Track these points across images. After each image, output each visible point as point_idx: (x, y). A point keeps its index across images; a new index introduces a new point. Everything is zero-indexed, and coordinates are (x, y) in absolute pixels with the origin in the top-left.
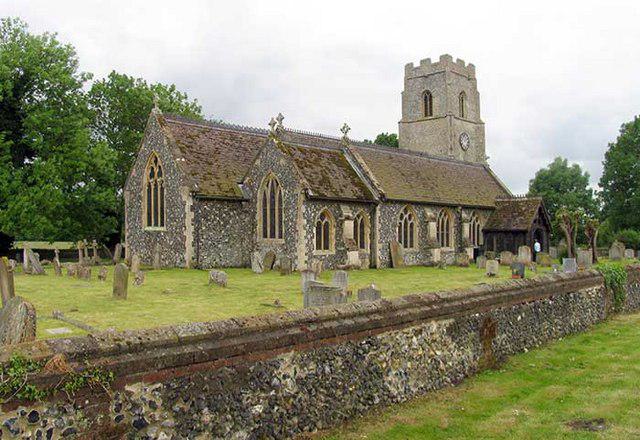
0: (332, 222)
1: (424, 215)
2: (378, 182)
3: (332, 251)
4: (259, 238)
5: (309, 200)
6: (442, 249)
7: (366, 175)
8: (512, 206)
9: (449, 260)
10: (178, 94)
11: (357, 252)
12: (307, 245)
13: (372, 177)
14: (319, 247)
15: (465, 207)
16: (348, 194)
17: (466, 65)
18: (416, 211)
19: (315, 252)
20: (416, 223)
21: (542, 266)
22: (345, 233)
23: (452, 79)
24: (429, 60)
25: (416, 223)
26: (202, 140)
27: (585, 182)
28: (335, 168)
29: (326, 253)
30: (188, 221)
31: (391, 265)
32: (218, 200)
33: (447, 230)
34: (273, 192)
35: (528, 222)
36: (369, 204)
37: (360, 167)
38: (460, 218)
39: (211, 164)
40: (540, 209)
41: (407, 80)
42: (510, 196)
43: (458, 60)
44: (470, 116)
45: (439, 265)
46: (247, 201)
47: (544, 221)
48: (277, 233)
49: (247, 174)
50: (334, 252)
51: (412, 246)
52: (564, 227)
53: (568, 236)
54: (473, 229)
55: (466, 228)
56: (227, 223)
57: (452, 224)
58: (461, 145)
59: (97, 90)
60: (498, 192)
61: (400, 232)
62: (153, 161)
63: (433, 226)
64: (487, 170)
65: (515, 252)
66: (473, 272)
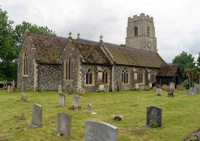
0: (93, 73)
1: (132, 71)
2: (113, 58)
3: (93, 85)
4: (65, 79)
5: (83, 64)
6: (140, 84)
7: (108, 54)
8: (167, 67)
9: (142, 88)
10: (49, 30)
11: (103, 85)
12: (82, 82)
13: (111, 55)
14: (87, 83)
15: (149, 68)
16: (100, 62)
17: (150, 17)
18: (129, 69)
19: (85, 85)
20: (129, 74)
21: (179, 90)
22: (98, 77)
23: (145, 22)
24: (136, 15)
25: (129, 74)
26: (45, 42)
27: (193, 60)
28: (96, 51)
29: (91, 85)
30: (35, 73)
31: (118, 90)
32: (48, 64)
33: (142, 76)
34: (70, 61)
35: (173, 73)
36: (109, 66)
37: (106, 52)
38: (147, 72)
39: (47, 51)
40: (178, 68)
41: (128, 23)
42: (166, 64)
43: (147, 15)
44: (151, 36)
45: (137, 90)
46: (60, 65)
47: (179, 73)
48: (71, 78)
49: (61, 54)
50: (94, 85)
51: (127, 83)
52: (188, 75)
53: (190, 78)
54: (152, 76)
55: (149, 75)
56: (52, 73)
57: (143, 74)
58: (148, 46)
59: (18, 28)
60: (162, 62)
61: (122, 77)
62: (26, 50)
63: (136, 74)
64: (158, 54)
65: (168, 85)
66: (152, 93)
